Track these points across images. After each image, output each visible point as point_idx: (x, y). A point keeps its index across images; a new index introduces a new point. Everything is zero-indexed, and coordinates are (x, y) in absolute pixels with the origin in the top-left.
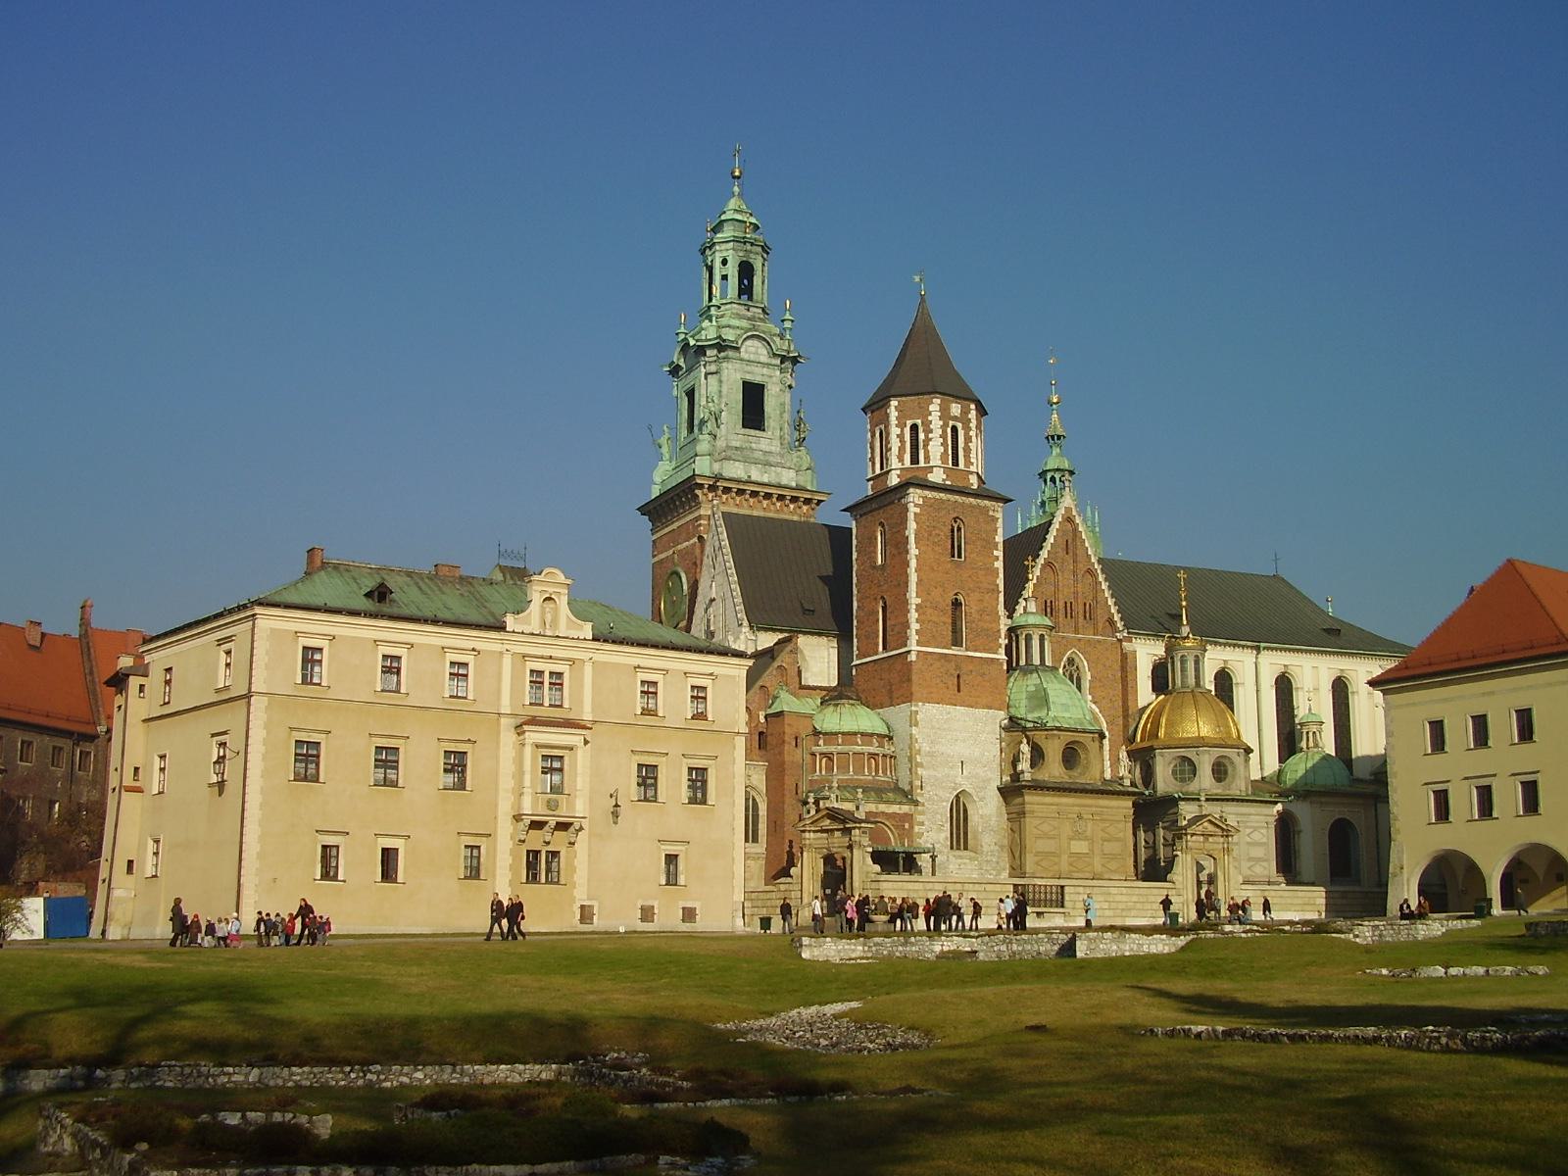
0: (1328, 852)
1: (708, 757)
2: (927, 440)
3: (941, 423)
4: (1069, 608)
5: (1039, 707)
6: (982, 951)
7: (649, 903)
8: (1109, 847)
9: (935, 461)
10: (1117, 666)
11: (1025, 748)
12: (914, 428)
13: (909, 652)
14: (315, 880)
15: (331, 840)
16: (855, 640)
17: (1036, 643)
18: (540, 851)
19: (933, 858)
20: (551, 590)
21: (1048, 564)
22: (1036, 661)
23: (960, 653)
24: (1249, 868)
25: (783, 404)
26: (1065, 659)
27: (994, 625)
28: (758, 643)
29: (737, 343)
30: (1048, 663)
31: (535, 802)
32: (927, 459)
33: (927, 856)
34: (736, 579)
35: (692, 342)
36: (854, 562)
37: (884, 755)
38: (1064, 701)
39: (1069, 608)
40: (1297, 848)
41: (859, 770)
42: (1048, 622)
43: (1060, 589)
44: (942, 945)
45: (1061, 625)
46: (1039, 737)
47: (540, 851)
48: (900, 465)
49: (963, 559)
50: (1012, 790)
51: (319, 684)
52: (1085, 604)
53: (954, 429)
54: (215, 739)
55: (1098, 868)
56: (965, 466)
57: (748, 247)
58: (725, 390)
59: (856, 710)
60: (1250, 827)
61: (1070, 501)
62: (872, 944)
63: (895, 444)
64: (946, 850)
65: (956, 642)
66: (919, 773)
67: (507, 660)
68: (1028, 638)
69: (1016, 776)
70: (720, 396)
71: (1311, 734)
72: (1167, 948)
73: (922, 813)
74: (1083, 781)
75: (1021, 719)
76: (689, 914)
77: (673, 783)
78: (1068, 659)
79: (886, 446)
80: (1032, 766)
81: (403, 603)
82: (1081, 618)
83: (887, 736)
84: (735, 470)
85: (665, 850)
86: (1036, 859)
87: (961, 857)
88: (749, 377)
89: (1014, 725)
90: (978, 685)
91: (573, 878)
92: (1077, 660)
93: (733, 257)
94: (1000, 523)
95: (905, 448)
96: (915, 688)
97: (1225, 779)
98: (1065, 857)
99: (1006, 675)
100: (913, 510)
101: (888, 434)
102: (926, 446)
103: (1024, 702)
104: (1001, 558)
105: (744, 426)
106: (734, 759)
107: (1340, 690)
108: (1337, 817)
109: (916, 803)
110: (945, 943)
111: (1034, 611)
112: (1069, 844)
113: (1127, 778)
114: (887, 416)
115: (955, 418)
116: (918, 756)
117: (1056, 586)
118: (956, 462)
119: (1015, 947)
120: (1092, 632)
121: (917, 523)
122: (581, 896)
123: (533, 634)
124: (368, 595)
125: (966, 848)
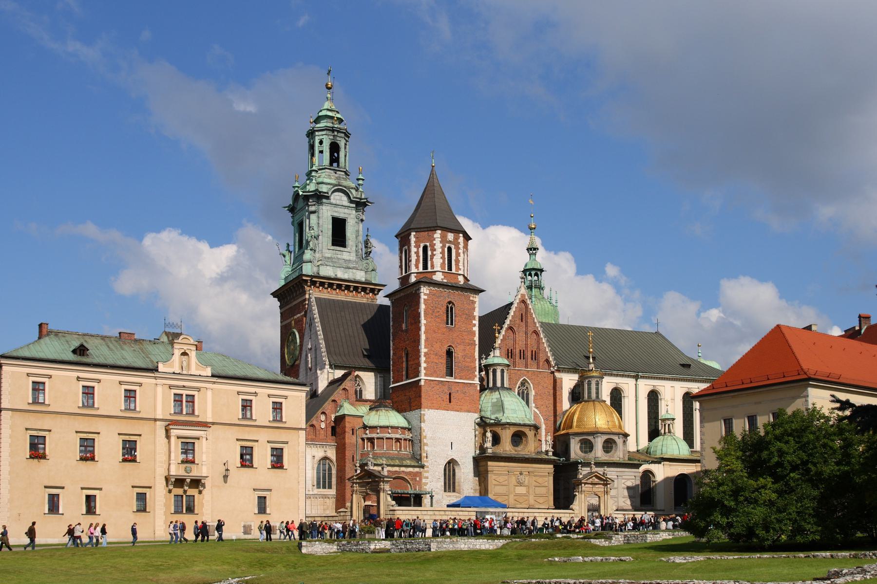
0: (673, 492)
2: (433, 255)
3: (441, 245)
4: (522, 353)
5: (498, 411)
7: (249, 523)
9: (437, 268)
10: (551, 387)
11: (489, 435)
12: (425, 249)
13: (420, 380)
14: (45, 514)
16: (392, 373)
19: (432, 497)
21: (510, 328)
22: (499, 384)
24: (624, 502)
25: (358, 231)
26: (519, 383)
27: (472, 364)
28: (335, 375)
29: (328, 193)
32: (433, 266)
33: (428, 496)
34: (322, 337)
35: (301, 193)
37: (405, 440)
38: (513, 408)
39: (522, 353)
40: (654, 491)
42: (506, 362)
43: (517, 342)
45: (517, 363)
46: (498, 430)
48: (416, 271)
49: (454, 326)
51: (44, 403)
52: (532, 351)
53: (450, 249)
55: (532, 502)
56: (456, 271)
57: (336, 133)
59: (388, 414)
61: (524, 290)
63: (414, 258)
67: (159, 389)
68: (494, 372)
69: (482, 449)
70: (318, 226)
71: (667, 426)
72: (466, 546)
73: (427, 472)
74: (524, 453)
75: (487, 418)
77: (262, 456)
78: (522, 383)
79: (409, 259)
80: (493, 445)
81: (96, 356)
82: (529, 359)
83: (407, 428)
84: (327, 271)
87: (450, 496)
88: (336, 215)
89: (483, 424)
90: (462, 399)
91: (202, 510)
94: (477, 305)
95: (419, 260)
96: (423, 400)
97: (611, 451)
99: (478, 394)
100: (423, 297)
101: (410, 251)
102: (432, 259)
103: (490, 409)
104: (477, 325)
105: (333, 244)
106: (299, 443)
109: (423, 467)
111: (499, 355)
115: (450, 242)
116: (425, 440)
117: (515, 341)
118: (450, 268)
120: (535, 368)
121: (426, 305)
123: (174, 373)
124: (74, 352)
125: (454, 491)
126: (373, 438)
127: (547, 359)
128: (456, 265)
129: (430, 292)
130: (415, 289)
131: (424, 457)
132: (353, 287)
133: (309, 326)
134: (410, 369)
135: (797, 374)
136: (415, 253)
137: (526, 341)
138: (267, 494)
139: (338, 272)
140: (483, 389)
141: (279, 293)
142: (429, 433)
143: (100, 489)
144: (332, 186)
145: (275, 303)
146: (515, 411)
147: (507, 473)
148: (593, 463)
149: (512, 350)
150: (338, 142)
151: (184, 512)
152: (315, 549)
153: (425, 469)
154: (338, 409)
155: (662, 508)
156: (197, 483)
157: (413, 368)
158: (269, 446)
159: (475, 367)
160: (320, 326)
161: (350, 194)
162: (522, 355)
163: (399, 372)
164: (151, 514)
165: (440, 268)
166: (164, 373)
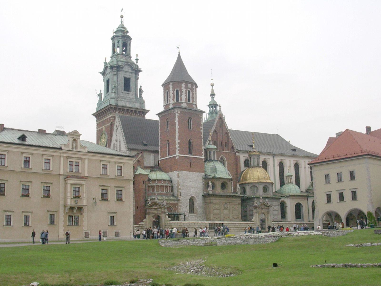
1: (123, 187)
2: (181, 95)
3: (185, 90)
4: (221, 144)
6: (218, 243)
8: (235, 212)
9: (184, 101)
11: (210, 184)
12: (177, 91)
13: (176, 156)
14: (4, 226)
15: (9, 213)
17: (212, 153)
19: (185, 216)
20: (75, 137)
23: (191, 156)
29: (122, 66)
30: (216, 159)
31: (71, 202)
32: (181, 100)
36: (159, 130)
37: (170, 186)
39: (221, 144)
40: (286, 212)
44: (205, 241)
48: (173, 102)
49: (192, 129)
50: (205, 196)
53: (189, 92)
54: (22, 183)
55: (231, 218)
57: (126, 38)
58: (119, 80)
59: (161, 173)
60: (274, 206)
62: (183, 242)
63: (171, 95)
64: (188, 214)
65: (190, 153)
67: (62, 159)
68: (210, 152)
71: (289, 179)
75: (209, 175)
76: (117, 234)
77: (112, 195)
79: (169, 96)
82: (224, 146)
85: (110, 215)
86: (273, 216)
87: (192, 215)
88: (126, 76)
89: (206, 179)
92: (223, 158)
93: (121, 40)
101: (170, 93)
102: (181, 96)
103: (209, 171)
104: (203, 129)
107: (297, 166)
109: (179, 200)
110: (206, 241)
112: (223, 211)
113: (239, 192)
114: (169, 87)
115: (189, 88)
117: (217, 137)
118: (189, 101)
119: (229, 241)
122: (85, 229)
124: (19, 138)
125: (193, 213)
126: (168, 186)
127: (232, 146)
129: (180, 113)
130: (173, 111)
133: (116, 129)
134: (171, 151)
135: (361, 152)
137: (222, 137)
138: (114, 215)
140: (205, 161)
141: (96, 114)
143: (32, 212)
144: (124, 63)
145: (95, 119)
146: (222, 172)
147: (220, 203)
148: (261, 197)
149: (216, 142)
150: (127, 42)
151: (74, 224)
152: (169, 244)
153: (180, 201)
154: (136, 171)
155: (290, 220)
156: (80, 209)
157: (172, 150)
158: (101, 188)
159: (202, 150)
160: (122, 129)
161: (132, 67)
162: (221, 144)
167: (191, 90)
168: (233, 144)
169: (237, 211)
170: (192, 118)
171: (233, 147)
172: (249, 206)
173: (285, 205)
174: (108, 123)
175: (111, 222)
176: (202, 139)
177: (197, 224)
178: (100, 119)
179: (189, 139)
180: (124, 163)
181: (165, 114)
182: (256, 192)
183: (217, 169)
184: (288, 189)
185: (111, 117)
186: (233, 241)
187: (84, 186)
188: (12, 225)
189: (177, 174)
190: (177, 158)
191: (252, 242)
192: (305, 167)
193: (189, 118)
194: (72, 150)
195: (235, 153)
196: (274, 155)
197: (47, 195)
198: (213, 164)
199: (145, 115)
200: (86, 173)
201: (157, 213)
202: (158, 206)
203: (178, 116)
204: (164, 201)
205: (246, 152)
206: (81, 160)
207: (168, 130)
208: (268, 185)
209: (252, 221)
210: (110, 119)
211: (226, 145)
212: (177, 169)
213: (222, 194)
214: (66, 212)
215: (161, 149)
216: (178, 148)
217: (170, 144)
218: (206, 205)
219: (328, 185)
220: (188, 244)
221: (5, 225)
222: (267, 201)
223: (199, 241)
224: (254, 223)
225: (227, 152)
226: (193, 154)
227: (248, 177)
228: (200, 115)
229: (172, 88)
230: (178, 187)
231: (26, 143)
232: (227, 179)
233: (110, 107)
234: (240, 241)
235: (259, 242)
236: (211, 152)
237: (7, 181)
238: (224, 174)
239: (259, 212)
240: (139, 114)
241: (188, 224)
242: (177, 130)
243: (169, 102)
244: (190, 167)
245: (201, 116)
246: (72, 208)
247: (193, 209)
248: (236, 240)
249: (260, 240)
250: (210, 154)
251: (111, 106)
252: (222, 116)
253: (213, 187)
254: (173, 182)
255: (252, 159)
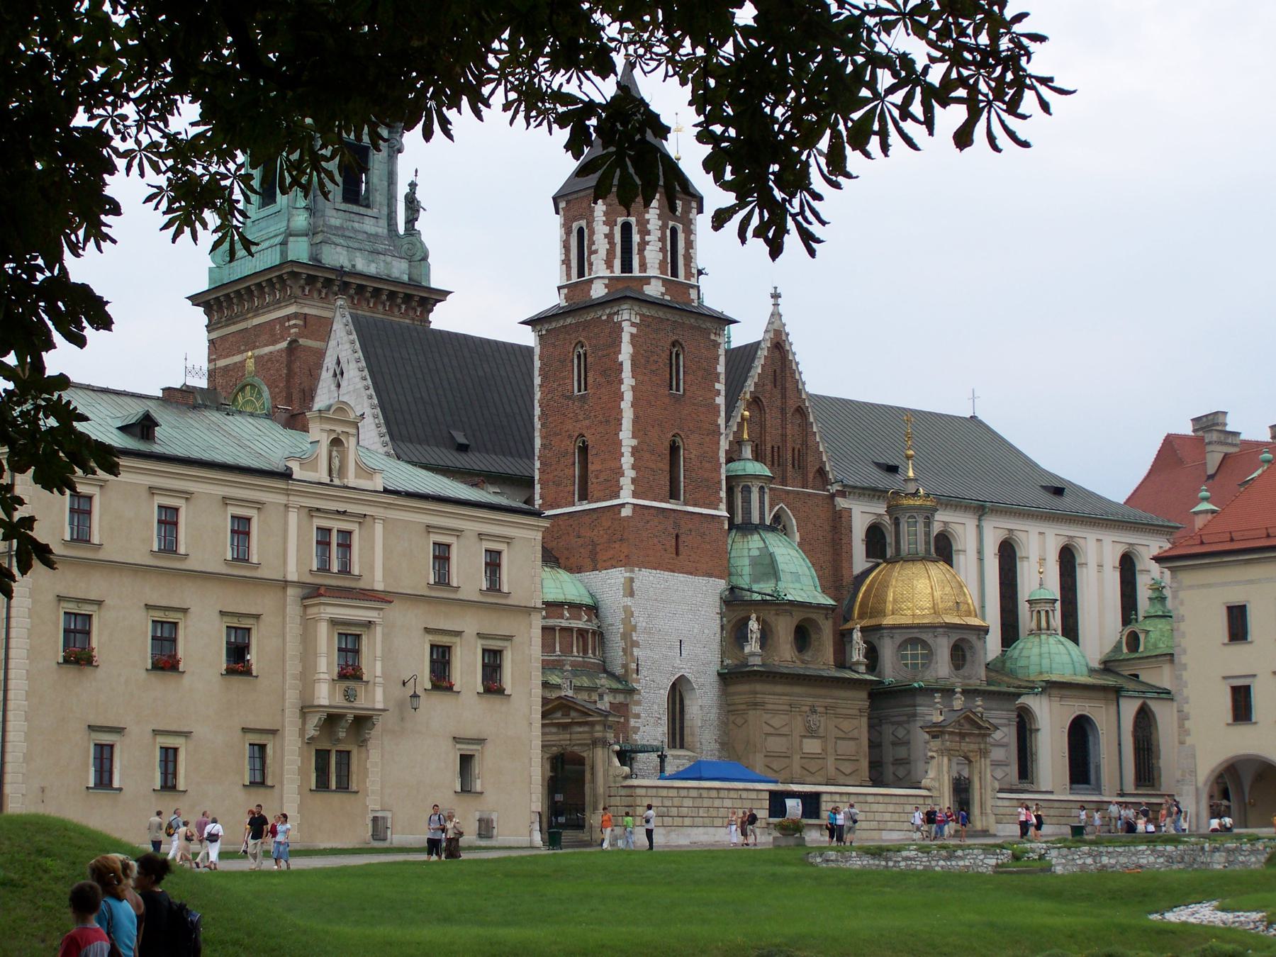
2: (643, 245)
3: (660, 223)
4: (776, 454)
6: (1059, 864)
9: (653, 271)
12: (626, 228)
13: (623, 505)
15: (170, 742)
17: (755, 496)
18: (329, 751)
20: (339, 429)
23: (679, 508)
27: (714, 474)
32: (643, 267)
36: (537, 389)
39: (776, 454)
41: (567, 650)
44: (997, 859)
47: (329, 751)
48: (607, 274)
50: (728, 678)
52: (793, 450)
62: (900, 859)
63: (601, 245)
65: (674, 495)
66: (635, 654)
67: (293, 517)
68: (747, 490)
71: (1043, 614)
79: (589, 248)
82: (790, 468)
83: (586, 606)
92: (784, 518)
98: (797, 758)
101: (592, 233)
102: (641, 251)
103: (747, 570)
104: (723, 393)
107: (1068, 559)
108: (1078, 713)
109: (632, 691)
112: (801, 741)
118: (675, 274)
120: (800, 485)
122: (373, 804)
125: (682, 747)
126: (587, 631)
127: (820, 467)
128: (685, 265)
131: (632, 670)
132: (386, 293)
134: (594, 481)
136: (606, 236)
137: (784, 428)
139: (356, 259)
142: (641, 619)
145: (199, 316)
146: (796, 577)
147: (789, 708)
148: (958, 690)
153: (636, 697)
156: (362, 722)
158: (429, 639)
159: (720, 482)
160: (368, 377)
163: (558, 485)
164: (276, 790)
165: (659, 272)
166: (305, 481)
167: (681, 226)
168: (824, 459)
169: (852, 743)
170: (684, 344)
171: (821, 472)
172: (893, 723)
173: (1031, 723)
174: (274, 343)
175: (165, 774)
176: (722, 434)
177: (726, 791)
178: (231, 321)
179: (672, 433)
180: (508, 540)
181: (569, 321)
182: (923, 665)
183: (781, 566)
184: (1040, 655)
185: (288, 318)
186: (1123, 860)
187: (379, 630)
188: (116, 784)
189: (623, 580)
190: (626, 512)
191: (1219, 863)
192: (1102, 566)
193: (674, 344)
194: (327, 480)
195: (833, 496)
196: (981, 510)
197: (238, 655)
198: (761, 545)
199: (431, 310)
200: (376, 578)
201: (568, 742)
202: (573, 714)
203: (632, 334)
204: (601, 697)
205: (874, 493)
206: (508, 543)
207: (579, 391)
208: (973, 638)
209: (920, 788)
210: (287, 324)
211: (796, 462)
212: (626, 562)
213: (799, 668)
214: (307, 737)
215: (542, 472)
216: (632, 474)
217: (591, 452)
218: (730, 712)
219: (1239, 649)
220: (925, 866)
221: (92, 785)
222: (979, 706)
223: (973, 858)
224: (931, 797)
225: (798, 493)
226: (684, 497)
227: (891, 599)
228: (715, 334)
229: (606, 214)
230: (626, 636)
231: (157, 449)
232: (819, 607)
233: (289, 270)
234: (1152, 859)
235: (1243, 862)
236: (750, 492)
237: (100, 604)
238: (804, 588)
239: (952, 752)
240: (404, 307)
241: (694, 793)
242: (628, 396)
243: (590, 275)
244: (674, 550)
245: (717, 338)
246: (332, 720)
247: (682, 728)
248: (1134, 854)
249: (1248, 858)
250: (747, 501)
251: (296, 270)
252: (784, 338)
253: (766, 636)
254: (602, 611)
255: (904, 527)
